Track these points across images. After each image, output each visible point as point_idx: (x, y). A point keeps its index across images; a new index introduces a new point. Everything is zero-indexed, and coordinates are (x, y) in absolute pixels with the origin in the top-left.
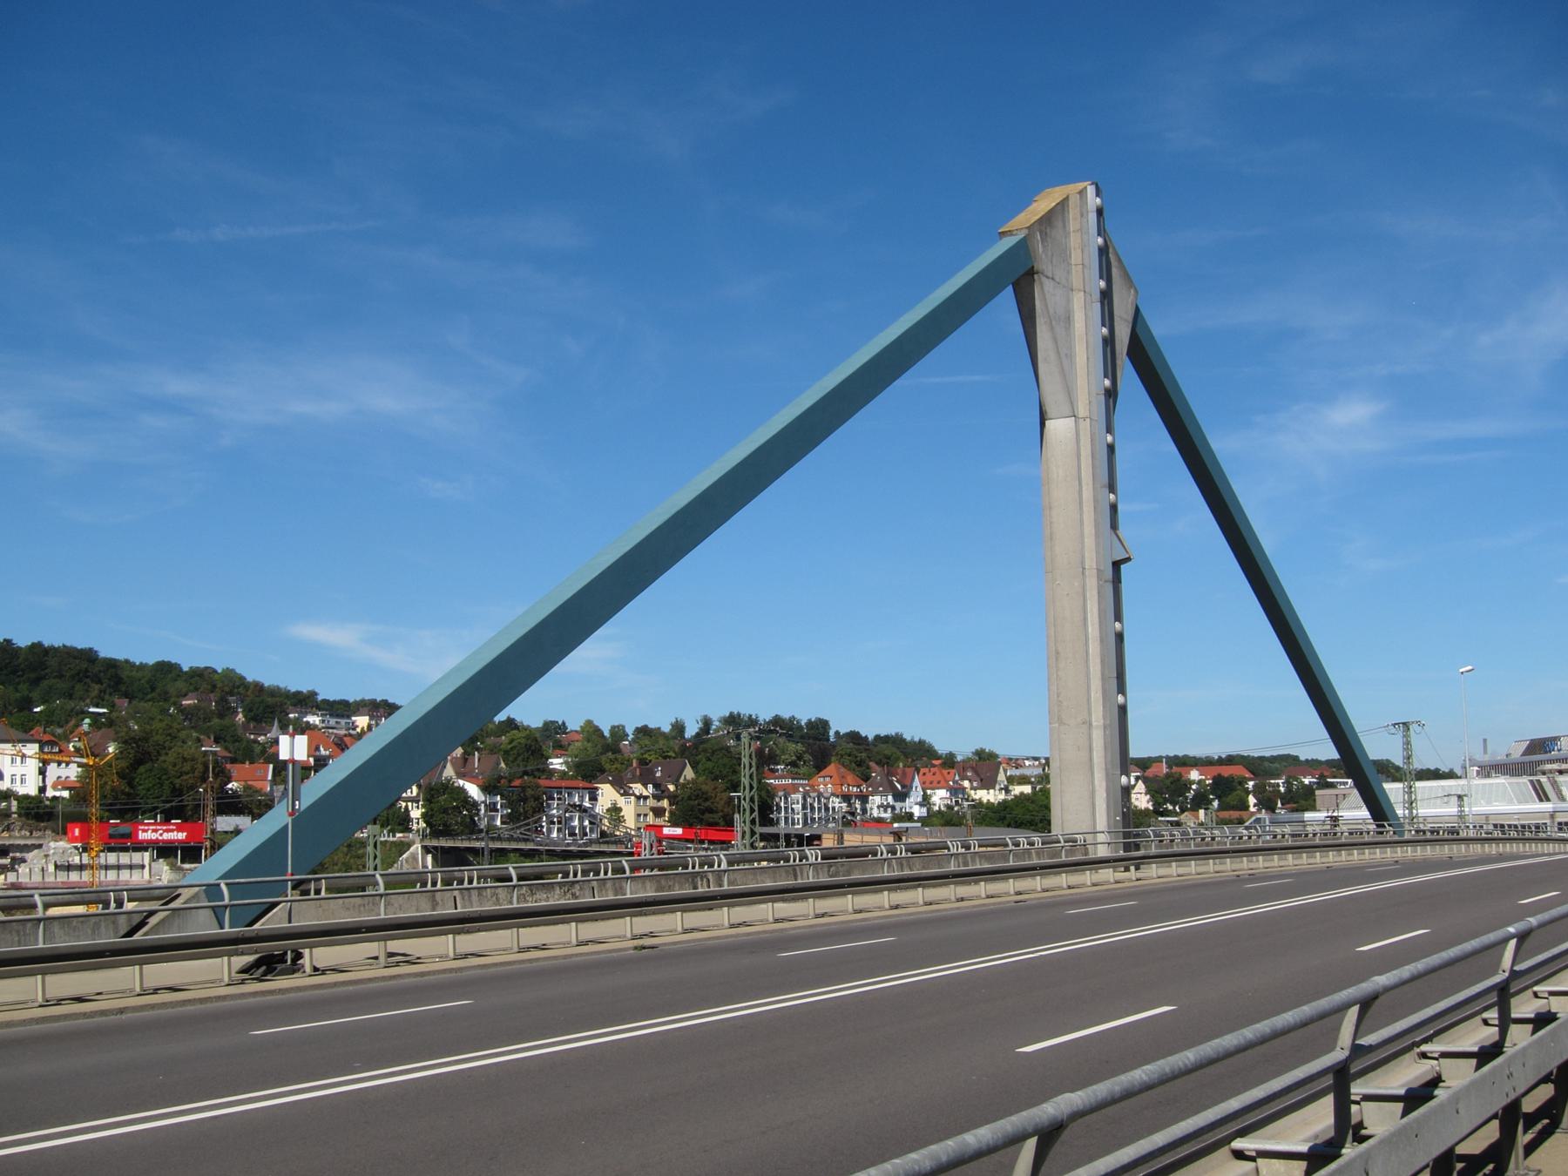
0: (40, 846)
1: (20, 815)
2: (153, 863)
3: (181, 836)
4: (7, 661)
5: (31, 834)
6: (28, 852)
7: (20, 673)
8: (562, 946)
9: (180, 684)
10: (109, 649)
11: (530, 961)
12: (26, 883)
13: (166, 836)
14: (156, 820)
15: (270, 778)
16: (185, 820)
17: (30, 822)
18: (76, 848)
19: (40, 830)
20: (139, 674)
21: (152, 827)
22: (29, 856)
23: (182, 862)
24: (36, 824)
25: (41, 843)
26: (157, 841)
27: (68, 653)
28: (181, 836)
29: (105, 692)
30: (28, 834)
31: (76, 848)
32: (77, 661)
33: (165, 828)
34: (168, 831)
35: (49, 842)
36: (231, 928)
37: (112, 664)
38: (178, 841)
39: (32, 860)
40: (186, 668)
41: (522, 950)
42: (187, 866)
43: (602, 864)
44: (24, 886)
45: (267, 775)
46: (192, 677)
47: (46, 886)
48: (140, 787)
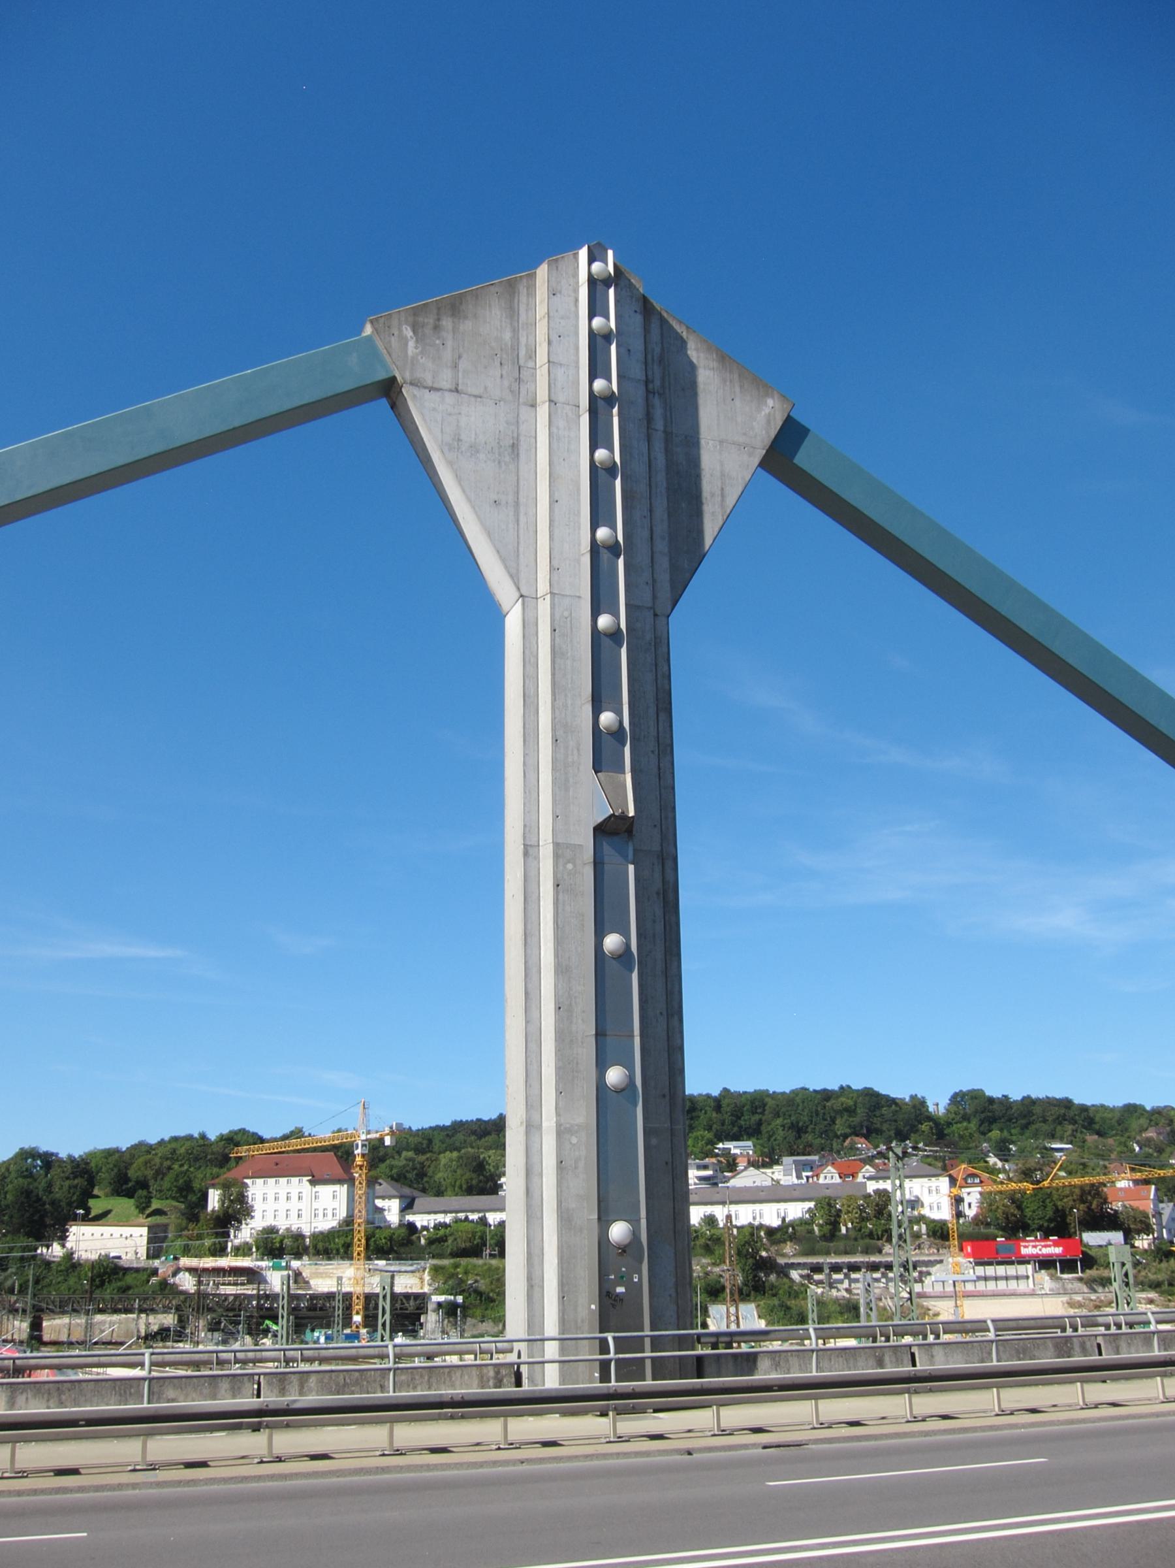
0: (941, 1262)
1: (928, 1236)
2: (1035, 1275)
3: (1058, 1250)
4: (1004, 1112)
5: (938, 1251)
6: (932, 1267)
7: (1014, 1121)
8: (1068, 1408)
9: (1143, 1121)
10: (1082, 1097)
11: (927, 1434)
12: (930, 1293)
13: (1045, 1251)
14: (1036, 1237)
15: (1152, 1197)
16: (1061, 1236)
17: (937, 1241)
18: (970, 1262)
19: (945, 1248)
20: (1110, 1116)
21: (1031, 1244)
22: (933, 1270)
23: (1062, 1272)
24: (942, 1242)
25: (941, 1258)
26: (1037, 1255)
27: (1049, 1103)
28: (1058, 1250)
29: (1076, 1131)
30: (935, 1251)
31: (970, 1262)
32: (1057, 1108)
33: (1043, 1244)
34: (1046, 1246)
35: (948, 1258)
36: (654, 1379)
37: (1084, 1109)
38: (1057, 1255)
39: (936, 1273)
40: (1148, 1108)
41: (1002, 1413)
42: (1065, 1276)
43: (928, 1326)
44: (928, 1294)
45: (1150, 1195)
46: (1153, 1115)
47: (946, 1295)
48: (1027, 1210)
